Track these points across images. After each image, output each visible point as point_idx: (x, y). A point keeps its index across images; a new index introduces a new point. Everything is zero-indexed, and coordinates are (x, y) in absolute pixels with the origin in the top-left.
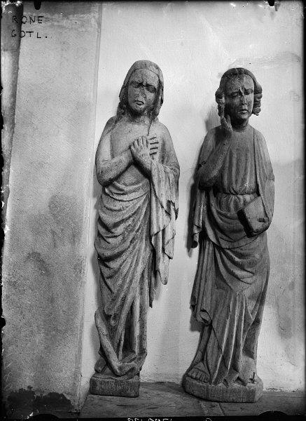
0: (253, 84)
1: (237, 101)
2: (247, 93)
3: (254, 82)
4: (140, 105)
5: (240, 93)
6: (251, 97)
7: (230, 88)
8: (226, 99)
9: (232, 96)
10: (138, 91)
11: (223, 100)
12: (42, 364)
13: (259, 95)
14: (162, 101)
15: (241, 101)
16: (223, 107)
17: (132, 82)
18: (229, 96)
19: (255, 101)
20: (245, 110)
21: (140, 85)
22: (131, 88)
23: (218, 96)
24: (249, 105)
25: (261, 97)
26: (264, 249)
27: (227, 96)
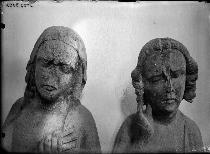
0: (185, 63)
1: (159, 87)
2: (174, 75)
3: (186, 58)
4: (51, 91)
5: (164, 77)
6: (182, 80)
7: (149, 70)
8: (144, 82)
9: (152, 80)
10: (47, 71)
11: (141, 84)
12: (51, 68)
13: (193, 77)
14: (84, 82)
15: (165, 87)
16: (141, 92)
17: (40, 59)
18: (148, 80)
19: (187, 84)
20: (172, 99)
21: (50, 63)
22: (38, 66)
23: (135, 78)
24: (177, 92)
25: (196, 79)
26: (29, 65)
27: (146, 79)
